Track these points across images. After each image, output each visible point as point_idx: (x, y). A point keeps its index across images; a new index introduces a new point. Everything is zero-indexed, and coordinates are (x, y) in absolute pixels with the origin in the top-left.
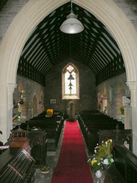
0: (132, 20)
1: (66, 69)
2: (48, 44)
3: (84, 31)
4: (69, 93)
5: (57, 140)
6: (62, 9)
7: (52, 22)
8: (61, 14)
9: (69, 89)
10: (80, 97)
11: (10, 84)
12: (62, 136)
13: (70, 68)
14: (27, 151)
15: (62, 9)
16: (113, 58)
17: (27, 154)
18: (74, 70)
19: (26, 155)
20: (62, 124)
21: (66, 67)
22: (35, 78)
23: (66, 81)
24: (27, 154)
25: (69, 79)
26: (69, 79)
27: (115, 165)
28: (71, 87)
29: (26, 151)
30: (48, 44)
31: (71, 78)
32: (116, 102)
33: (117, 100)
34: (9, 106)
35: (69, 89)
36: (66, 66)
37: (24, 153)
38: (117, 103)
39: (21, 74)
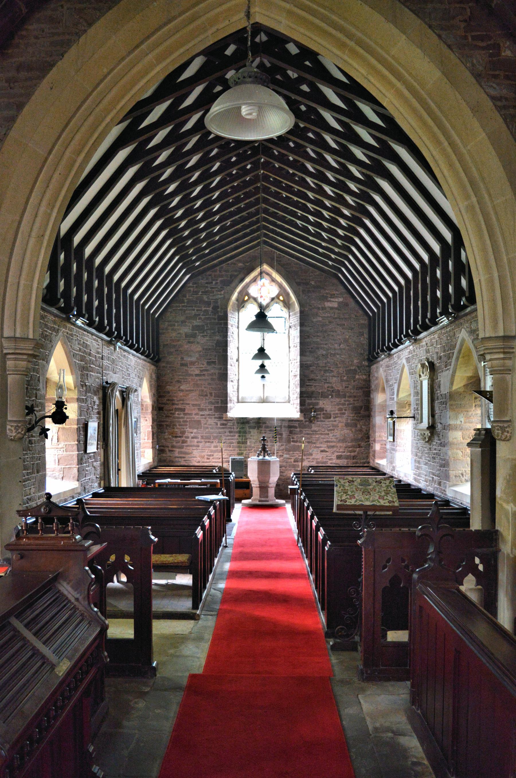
0: (500, 99)
1: (248, 294)
2: (172, 188)
3: (296, 125)
4: (258, 394)
5: (201, 572)
6: (230, 51)
7: (189, 101)
8: (222, 64)
9: (258, 372)
10: (301, 411)
11: (15, 339)
12: (223, 564)
13: (265, 287)
14: (76, 588)
15: (230, 51)
16: (436, 247)
17: (77, 599)
18: (278, 297)
19: (73, 600)
20: (225, 512)
21: (248, 285)
22: (118, 328)
23: (241, 340)
24: (77, 599)
25: (253, 326)
26: (253, 326)
27: (222, 265)
28: (262, 366)
29: (70, 589)
30: (172, 188)
31: (261, 322)
32: (447, 427)
33: (452, 422)
34: (8, 427)
35: (258, 372)
36: (247, 280)
37: (66, 593)
38: (450, 432)
39: (60, 309)
